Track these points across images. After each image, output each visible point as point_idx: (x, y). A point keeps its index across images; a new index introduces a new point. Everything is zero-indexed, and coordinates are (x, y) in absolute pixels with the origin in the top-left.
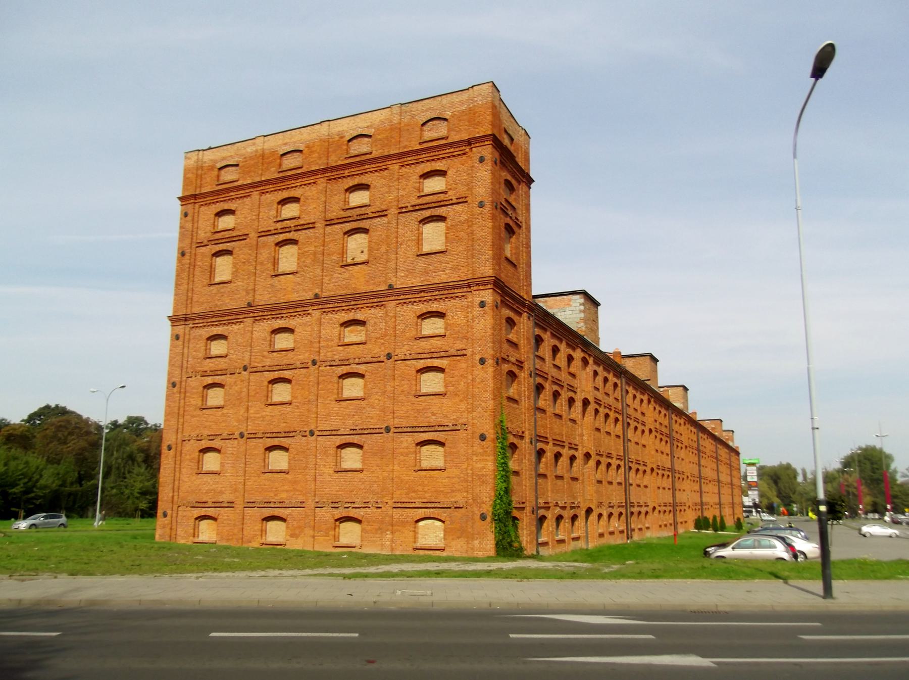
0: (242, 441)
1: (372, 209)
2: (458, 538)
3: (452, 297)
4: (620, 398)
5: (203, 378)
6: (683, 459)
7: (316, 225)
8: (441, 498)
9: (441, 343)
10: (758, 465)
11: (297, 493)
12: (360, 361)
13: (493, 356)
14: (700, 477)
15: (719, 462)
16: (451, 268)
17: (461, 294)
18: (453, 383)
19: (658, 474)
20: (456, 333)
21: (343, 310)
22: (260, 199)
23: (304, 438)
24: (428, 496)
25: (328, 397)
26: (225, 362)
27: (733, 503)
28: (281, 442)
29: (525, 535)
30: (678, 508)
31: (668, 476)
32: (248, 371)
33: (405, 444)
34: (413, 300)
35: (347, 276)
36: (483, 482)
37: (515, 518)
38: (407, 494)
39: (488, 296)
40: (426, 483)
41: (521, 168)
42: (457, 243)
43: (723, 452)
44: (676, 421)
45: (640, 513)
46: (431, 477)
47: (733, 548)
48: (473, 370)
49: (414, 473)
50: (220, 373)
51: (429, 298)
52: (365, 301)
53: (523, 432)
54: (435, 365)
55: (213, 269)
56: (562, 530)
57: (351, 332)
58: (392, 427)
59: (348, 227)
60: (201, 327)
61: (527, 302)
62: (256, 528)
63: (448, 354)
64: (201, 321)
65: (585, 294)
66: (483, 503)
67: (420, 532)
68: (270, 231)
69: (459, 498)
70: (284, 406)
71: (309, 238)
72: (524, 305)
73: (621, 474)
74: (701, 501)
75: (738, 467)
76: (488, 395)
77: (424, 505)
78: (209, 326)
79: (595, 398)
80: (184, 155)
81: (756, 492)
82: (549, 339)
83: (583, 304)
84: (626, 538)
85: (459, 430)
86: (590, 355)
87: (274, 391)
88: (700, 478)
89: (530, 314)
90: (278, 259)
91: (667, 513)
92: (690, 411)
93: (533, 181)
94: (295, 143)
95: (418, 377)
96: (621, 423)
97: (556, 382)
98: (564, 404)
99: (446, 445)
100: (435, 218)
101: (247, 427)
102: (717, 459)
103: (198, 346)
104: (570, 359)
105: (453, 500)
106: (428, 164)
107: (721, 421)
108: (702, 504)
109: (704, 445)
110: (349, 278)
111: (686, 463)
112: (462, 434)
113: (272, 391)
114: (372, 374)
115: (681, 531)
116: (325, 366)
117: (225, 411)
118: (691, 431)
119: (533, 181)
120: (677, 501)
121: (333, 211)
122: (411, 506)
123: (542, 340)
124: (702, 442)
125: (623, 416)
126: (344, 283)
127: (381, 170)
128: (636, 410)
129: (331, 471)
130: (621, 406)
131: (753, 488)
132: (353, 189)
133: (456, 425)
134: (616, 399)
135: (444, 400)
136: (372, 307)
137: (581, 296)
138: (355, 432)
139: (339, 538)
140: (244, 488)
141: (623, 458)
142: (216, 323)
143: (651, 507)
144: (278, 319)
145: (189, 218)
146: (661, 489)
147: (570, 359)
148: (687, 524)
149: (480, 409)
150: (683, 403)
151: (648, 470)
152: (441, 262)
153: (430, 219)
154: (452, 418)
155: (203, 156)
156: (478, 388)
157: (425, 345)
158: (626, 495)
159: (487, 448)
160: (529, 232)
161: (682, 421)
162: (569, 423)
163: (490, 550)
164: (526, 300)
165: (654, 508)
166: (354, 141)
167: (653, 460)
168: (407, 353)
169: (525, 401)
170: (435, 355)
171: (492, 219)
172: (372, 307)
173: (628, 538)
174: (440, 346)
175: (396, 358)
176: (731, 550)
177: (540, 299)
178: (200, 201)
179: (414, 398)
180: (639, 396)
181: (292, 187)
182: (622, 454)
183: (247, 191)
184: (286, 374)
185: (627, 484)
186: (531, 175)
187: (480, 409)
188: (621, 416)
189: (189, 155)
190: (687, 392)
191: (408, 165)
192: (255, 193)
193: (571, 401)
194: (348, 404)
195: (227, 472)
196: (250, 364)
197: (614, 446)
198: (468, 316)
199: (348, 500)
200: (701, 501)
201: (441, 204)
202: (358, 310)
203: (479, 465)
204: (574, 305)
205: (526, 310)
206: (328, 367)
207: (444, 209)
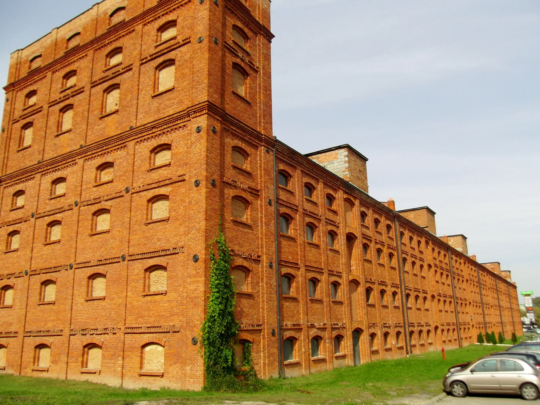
0: (26, 278)
1: (122, 66)
2: (175, 363)
3: (176, 129)
4: (394, 237)
5: (8, 227)
6: (464, 290)
7: (85, 89)
8: (162, 323)
9: (166, 172)
10: (534, 296)
11: (59, 322)
12: (108, 198)
13: (207, 177)
14: (482, 303)
15: (499, 293)
16: (178, 103)
17: (182, 124)
18: (175, 208)
19: (473, 305)
20: (178, 161)
21: (98, 155)
22: (52, 77)
23: (67, 272)
24: (152, 321)
25: (84, 233)
26: (22, 212)
27: (513, 322)
28: (51, 276)
29: (262, 358)
30: (488, 326)
31: (480, 306)
32: (34, 218)
33: (136, 271)
34: (147, 137)
35: (103, 127)
36: (195, 304)
37: (244, 342)
38: (136, 319)
39: (203, 121)
40: (151, 308)
41: (258, 23)
42: (182, 79)
43: (502, 286)
44: (482, 274)
45: (449, 330)
46: (155, 302)
47: (472, 371)
48: (189, 194)
49: (142, 299)
50: (18, 221)
51: (159, 132)
52: (114, 145)
53: (259, 257)
54: (161, 193)
55: (22, 139)
56: (322, 350)
57: (106, 174)
58: (127, 255)
59: (106, 85)
60: (10, 186)
61: (263, 137)
62: (30, 356)
63: (171, 181)
64: (9, 181)
65: (428, 209)
66: (195, 326)
67: (146, 358)
68: (56, 100)
69: (176, 322)
70: (55, 244)
71: (80, 100)
72: (260, 140)
73: (399, 300)
74: (484, 321)
75: (516, 296)
76: (202, 216)
77: (149, 331)
78: (14, 184)
79: (363, 234)
80: (10, 56)
81: (532, 314)
82: (407, 234)
83: (348, 156)
84: (405, 353)
85: (178, 253)
86: (355, 198)
87: (53, 233)
88: (482, 305)
89: (268, 148)
90: (62, 123)
91: (451, 331)
92: (470, 254)
93: (273, 36)
94: (76, 27)
95: (150, 206)
96: (396, 258)
97: (413, 256)
98: (321, 235)
99: (168, 269)
100: (168, 63)
101: (31, 265)
102: (497, 290)
103: (7, 202)
104: (419, 242)
105: (171, 324)
106: (164, 17)
107: (499, 264)
108: (485, 323)
109: (500, 287)
110: (105, 128)
111: (490, 298)
112: (180, 257)
113: (50, 232)
114: (116, 208)
115: (465, 344)
116: (84, 206)
117: (19, 253)
118: (472, 269)
119: (273, 36)
120: (460, 321)
121: (97, 75)
122: (138, 332)
123: (379, 222)
124: (498, 285)
125: (450, 272)
126: (101, 132)
127: (130, 32)
128: (457, 269)
129: (83, 301)
130: (395, 244)
131: (529, 312)
132: (112, 54)
133: (175, 249)
134: (446, 264)
135: (168, 226)
136: (118, 149)
137: (346, 149)
138: (101, 263)
139: (87, 364)
140: (25, 319)
141: (399, 286)
142: (18, 181)
143: (433, 326)
144: (57, 171)
145: (9, 102)
146: (443, 312)
147: (419, 242)
148: (472, 339)
149: (194, 231)
150: (463, 248)
151: (429, 297)
152: (169, 99)
153: (163, 65)
154: (173, 242)
155: (21, 54)
156: (193, 210)
157: (155, 176)
158: (404, 317)
159: (200, 269)
160: (269, 77)
161: (462, 261)
162: (329, 252)
163: (199, 377)
164: (262, 135)
165: (436, 328)
166: (115, 15)
167: (434, 289)
168: (141, 185)
169: (262, 227)
170: (162, 184)
171: (209, 51)
172: (118, 149)
173: (407, 353)
174: (165, 175)
175: (133, 191)
176: (470, 373)
177: (313, 156)
178: (17, 87)
179: (145, 227)
180: (459, 260)
181: (72, 63)
182: (398, 283)
183: (45, 73)
184: (58, 217)
185: (405, 308)
186: (271, 32)
187: (194, 231)
188: (396, 252)
189: (13, 55)
190: (364, 165)
191: (148, 23)
192: (49, 73)
193: (422, 266)
194: (98, 237)
195: (16, 305)
196: (37, 212)
197: (449, 292)
198: (188, 143)
199: (92, 327)
200: (484, 321)
201: (171, 49)
202: (109, 154)
203: (192, 287)
204: (340, 157)
205: (263, 144)
206: (86, 207)
207: (174, 52)
